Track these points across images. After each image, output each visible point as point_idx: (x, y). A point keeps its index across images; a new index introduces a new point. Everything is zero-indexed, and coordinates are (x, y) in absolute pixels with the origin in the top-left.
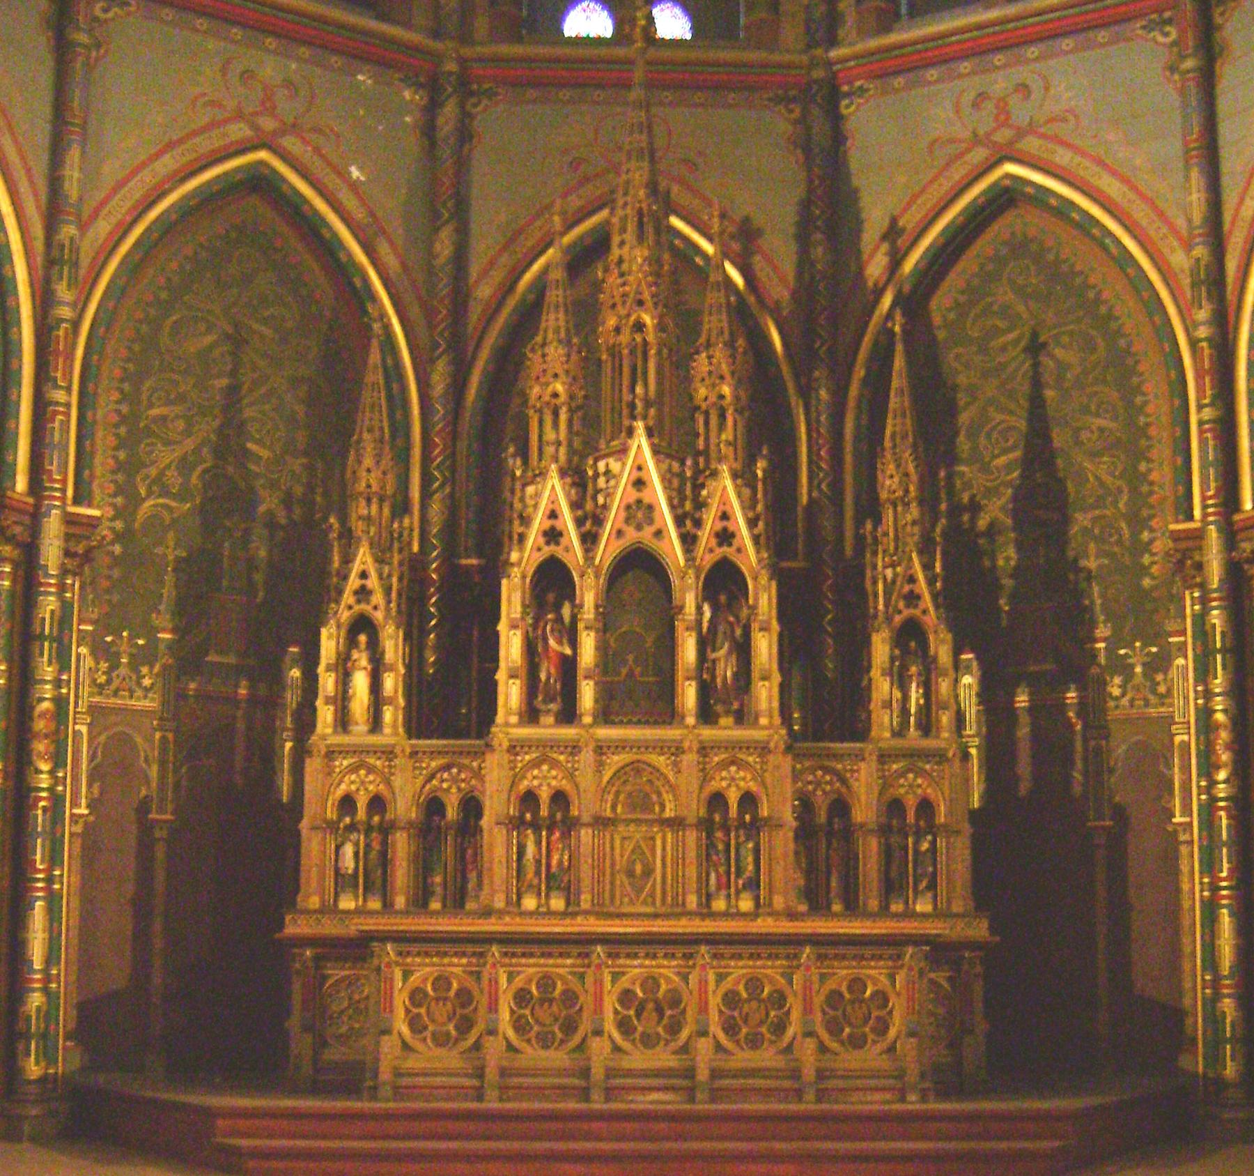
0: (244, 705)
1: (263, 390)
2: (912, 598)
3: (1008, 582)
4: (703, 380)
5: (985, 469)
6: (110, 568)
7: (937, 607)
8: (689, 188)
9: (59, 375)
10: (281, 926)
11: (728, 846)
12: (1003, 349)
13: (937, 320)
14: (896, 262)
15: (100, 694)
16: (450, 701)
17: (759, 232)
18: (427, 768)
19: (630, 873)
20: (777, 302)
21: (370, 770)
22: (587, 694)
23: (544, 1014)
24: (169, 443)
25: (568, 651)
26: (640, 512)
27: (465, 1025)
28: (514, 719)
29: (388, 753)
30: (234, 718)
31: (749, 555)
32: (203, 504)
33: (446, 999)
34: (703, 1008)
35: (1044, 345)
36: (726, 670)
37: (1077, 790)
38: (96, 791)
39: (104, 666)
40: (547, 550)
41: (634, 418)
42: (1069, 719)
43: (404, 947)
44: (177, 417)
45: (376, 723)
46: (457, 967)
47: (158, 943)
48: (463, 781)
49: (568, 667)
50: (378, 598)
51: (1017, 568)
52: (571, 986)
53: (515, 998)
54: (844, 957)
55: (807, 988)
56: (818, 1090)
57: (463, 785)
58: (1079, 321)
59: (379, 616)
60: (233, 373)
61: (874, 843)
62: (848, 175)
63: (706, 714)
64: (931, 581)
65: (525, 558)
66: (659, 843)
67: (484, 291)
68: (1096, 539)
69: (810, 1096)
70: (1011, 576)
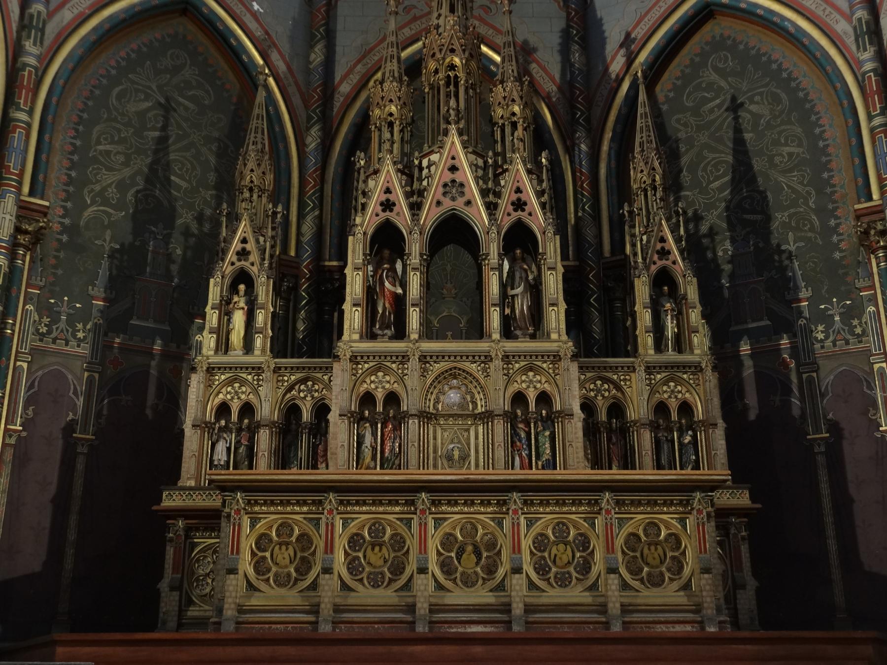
0: (157, 358)
1: (185, 143)
2: (664, 253)
4: (500, 103)
6: (57, 250)
7: (683, 259)
9: (22, 101)
10: (160, 500)
11: (528, 434)
12: (711, 111)
14: (630, 61)
17: (535, 50)
18: (287, 381)
20: (549, 93)
21: (243, 382)
22: (414, 318)
23: (375, 557)
24: (110, 169)
26: (454, 187)
28: (356, 337)
29: (257, 369)
30: (149, 366)
31: (538, 219)
32: (135, 213)
33: (287, 544)
34: (516, 548)
35: (742, 104)
36: (522, 305)
38: (30, 412)
39: (46, 320)
40: (383, 216)
41: (449, 123)
42: (784, 359)
44: (118, 153)
45: (248, 346)
47: (72, 536)
48: (316, 391)
49: (399, 303)
50: (254, 257)
52: (400, 531)
53: (349, 542)
54: (640, 503)
55: (608, 527)
56: (624, 623)
57: (316, 395)
59: (255, 269)
60: (164, 128)
61: (647, 437)
62: (595, 11)
63: (507, 333)
64: (678, 240)
65: (366, 222)
66: (472, 433)
67: (345, 88)
70: (729, 262)
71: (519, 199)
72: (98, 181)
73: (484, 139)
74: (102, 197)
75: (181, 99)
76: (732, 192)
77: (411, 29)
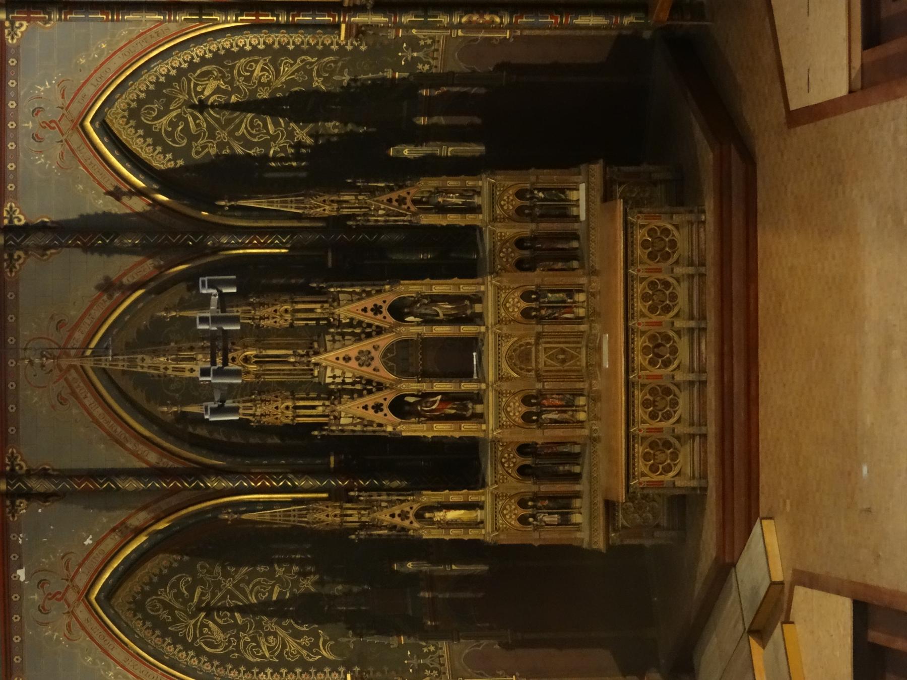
1: (237, 593)
3: (350, 127)
5: (274, 138)
8: (77, 326)
11: (549, 308)
13: (171, 165)
15: (444, 673)
16: (457, 465)
17: (107, 279)
19: (563, 361)
20: (156, 267)
23: (660, 405)
24: (284, 646)
25: (439, 397)
27: (667, 444)
31: (388, 296)
35: (200, 101)
37: (482, 91)
39: (427, 672)
40: (386, 410)
43: (631, 477)
44: (267, 641)
46: (639, 449)
49: (448, 397)
51: (340, 122)
58: (189, 81)
59: (416, 506)
60: (231, 610)
64: (392, 190)
65: (390, 423)
67: (153, 458)
68: (331, 75)
69: (702, 270)
71: (372, 310)
72: (298, 653)
73: (314, 336)
74: (312, 648)
75: (196, 600)
76: (281, 117)
77: (86, 397)
